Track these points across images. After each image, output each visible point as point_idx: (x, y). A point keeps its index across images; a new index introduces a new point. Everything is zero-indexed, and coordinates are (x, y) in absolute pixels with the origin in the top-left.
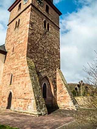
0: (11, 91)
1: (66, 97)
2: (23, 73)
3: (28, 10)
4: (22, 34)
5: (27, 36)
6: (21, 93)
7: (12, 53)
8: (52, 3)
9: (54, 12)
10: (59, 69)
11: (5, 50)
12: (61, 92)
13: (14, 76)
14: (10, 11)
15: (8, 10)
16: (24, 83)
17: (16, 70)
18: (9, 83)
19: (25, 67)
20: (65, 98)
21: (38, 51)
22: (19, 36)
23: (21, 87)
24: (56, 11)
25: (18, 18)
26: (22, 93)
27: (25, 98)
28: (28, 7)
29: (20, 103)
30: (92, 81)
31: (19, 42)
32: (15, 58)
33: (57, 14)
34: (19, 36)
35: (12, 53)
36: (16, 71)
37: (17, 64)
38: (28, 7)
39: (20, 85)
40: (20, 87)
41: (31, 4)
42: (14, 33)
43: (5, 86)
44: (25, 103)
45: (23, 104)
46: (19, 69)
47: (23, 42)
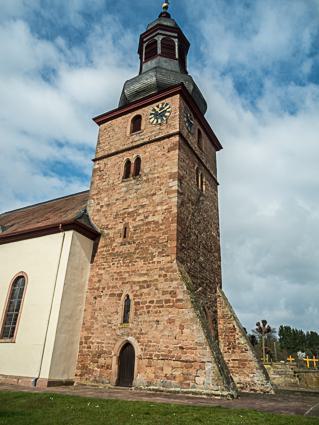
0: (131, 339)
1: (246, 360)
2: (168, 297)
3: (168, 143)
4: (154, 198)
5: (175, 210)
7: (120, 240)
8: (203, 115)
10: (221, 287)
12: (232, 347)
13: (137, 303)
14: (99, 124)
15: (94, 119)
16: (178, 323)
17: (142, 287)
18: (119, 318)
19: (175, 283)
20: (243, 363)
22: (145, 201)
24: (211, 140)
26: (172, 346)
28: (169, 136)
29: (168, 371)
30: (308, 326)
31: (147, 217)
32: (136, 256)
33: (213, 149)
34: (145, 201)
35: (120, 240)
36: (145, 291)
37: (144, 272)
38: (169, 136)
39: (161, 327)
40: (162, 331)
41: (179, 134)
44: (185, 371)
45: (177, 373)
46: (153, 288)
47: (160, 222)
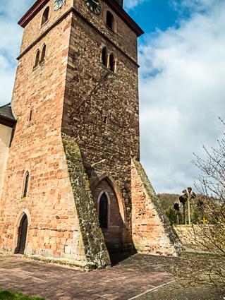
0: (27, 211)
1: (153, 225)
2: (52, 169)
3: (65, 22)
4: (51, 78)
5: (64, 84)
6: (48, 217)
7: (27, 123)
8: (122, 8)
9: (125, 28)
10: (138, 159)
11: (13, 116)
12: (142, 213)
13: (33, 178)
14: (23, 26)
16: (57, 193)
17: (37, 163)
18: (21, 192)
19: (58, 156)
20: (150, 228)
21: (89, 118)
22: (45, 83)
23: (48, 203)
24: (129, 26)
25: (42, 42)
26: (51, 216)
27: (58, 228)
28: (65, 16)
29: (46, 240)
30: (213, 188)
31: (45, 98)
32: (35, 135)
33: (133, 34)
34: (45, 83)
35: (27, 123)
36: (38, 165)
37: (39, 148)
38: (65, 16)
39: (45, 198)
40: (46, 201)
41: (73, 10)
42: (33, 77)
43: (12, 201)
44: (58, 240)
45: (52, 242)
46: (43, 161)
47: (53, 99)
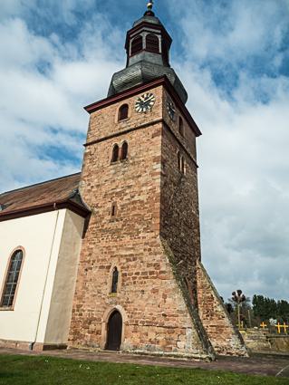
0: (119, 307)
1: (222, 327)
2: (152, 269)
6: (151, 314)
9: (189, 131)
10: (200, 260)
11: (81, 202)
14: (90, 112)
15: (85, 108)
16: (161, 293)
17: (128, 260)
18: (107, 289)
19: (158, 257)
20: (220, 329)
21: (173, 221)
23: (150, 302)
24: (191, 127)
25: (126, 138)
27: (165, 325)
28: (153, 124)
29: (152, 336)
30: (279, 296)
31: (133, 197)
33: (193, 135)
34: (131, 182)
35: (109, 217)
37: (131, 246)
39: (145, 296)
40: (147, 300)
41: (162, 121)
42: (113, 171)
43: (94, 295)
44: (168, 336)
47: (145, 201)
